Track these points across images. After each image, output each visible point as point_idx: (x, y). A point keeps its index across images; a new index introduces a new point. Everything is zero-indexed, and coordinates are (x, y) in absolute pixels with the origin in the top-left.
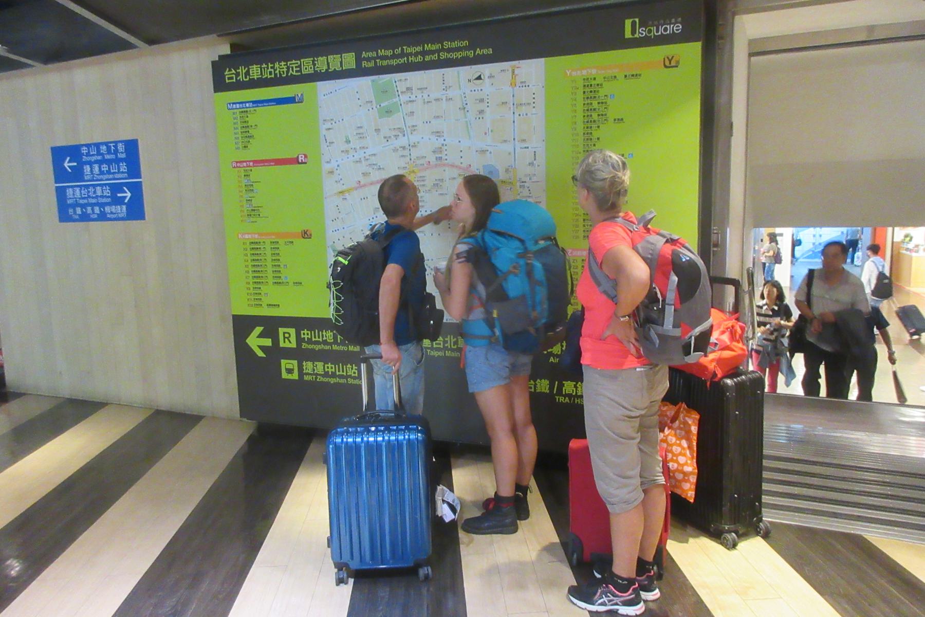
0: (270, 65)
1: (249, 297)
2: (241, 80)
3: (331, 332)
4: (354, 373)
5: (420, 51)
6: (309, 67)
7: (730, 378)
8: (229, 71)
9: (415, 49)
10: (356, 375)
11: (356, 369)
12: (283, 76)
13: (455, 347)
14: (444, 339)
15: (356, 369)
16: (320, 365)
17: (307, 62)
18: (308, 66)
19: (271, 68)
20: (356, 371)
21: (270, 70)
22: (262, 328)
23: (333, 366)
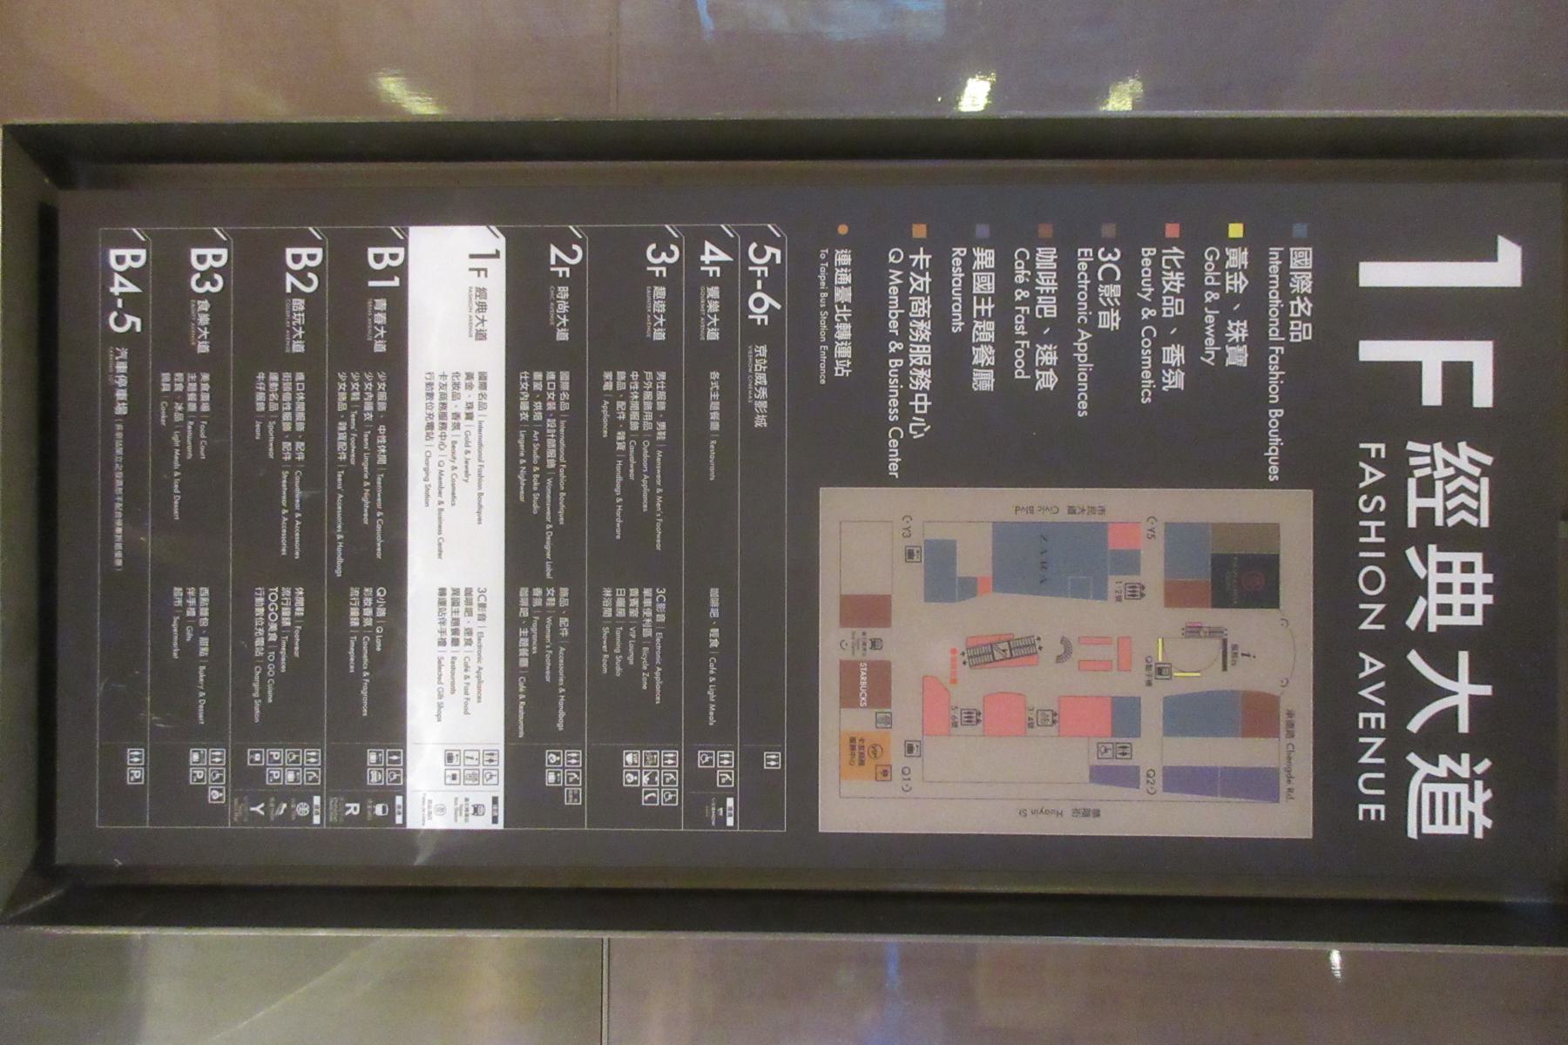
0: (765, 368)
1: (449, 592)
6: (1299, 334)
7: (254, 641)
11: (845, 373)
13: (836, 319)
15: (845, 373)
16: (1052, 286)
20: (842, 375)
23: (925, 411)
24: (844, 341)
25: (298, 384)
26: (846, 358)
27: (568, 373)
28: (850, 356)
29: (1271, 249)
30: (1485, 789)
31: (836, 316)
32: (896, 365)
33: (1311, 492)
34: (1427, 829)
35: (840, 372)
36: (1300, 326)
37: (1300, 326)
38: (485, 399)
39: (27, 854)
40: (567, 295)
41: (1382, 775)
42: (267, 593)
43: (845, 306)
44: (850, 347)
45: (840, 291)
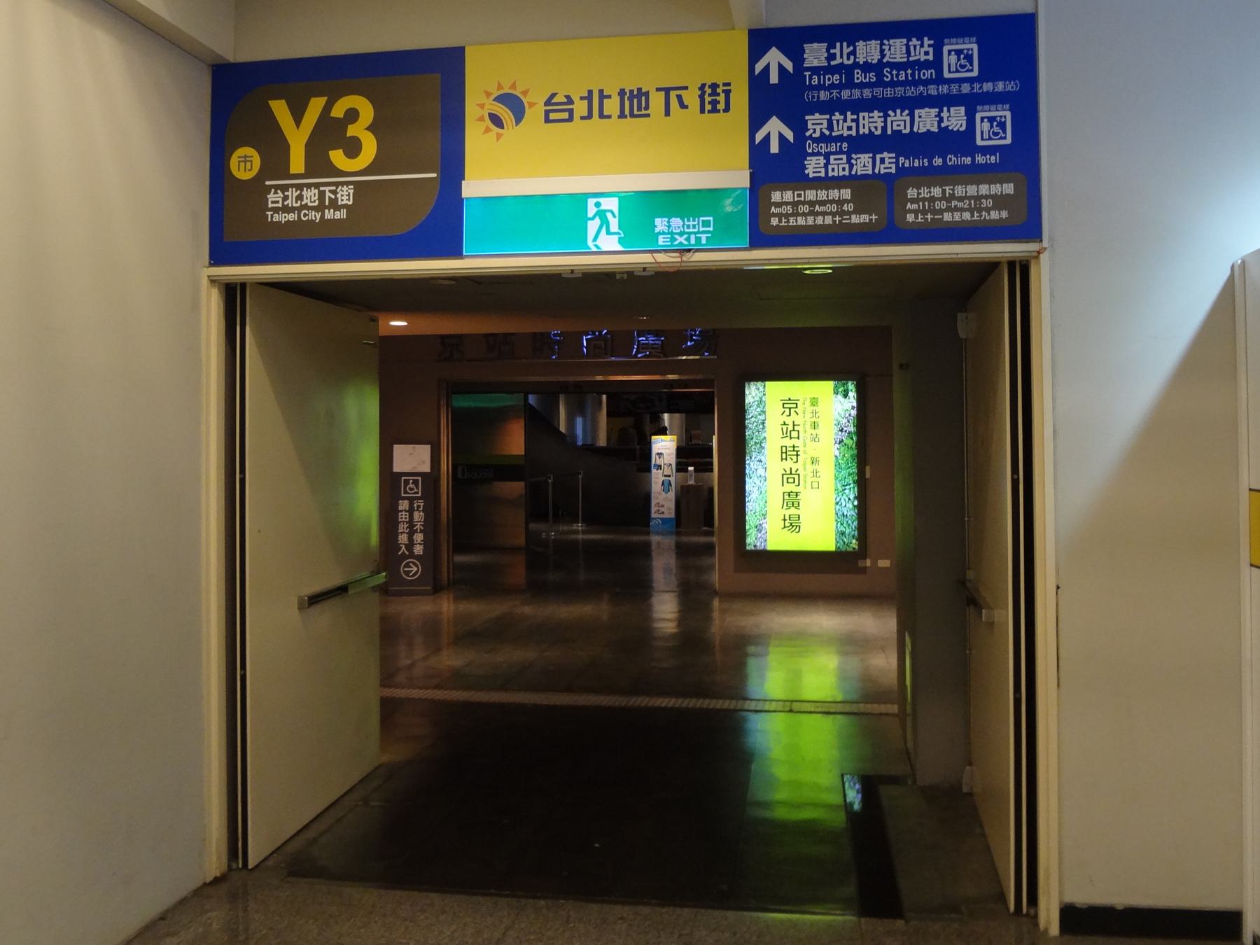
3: (315, 189)
5: (292, 219)
6: (841, 167)
8: (275, 193)
9: (285, 217)
12: (876, 133)
14: (284, 194)
15: (929, 46)
17: (959, 115)
18: (838, 165)
19: (853, 120)
21: (849, 123)
22: (791, 140)
25: (796, 199)
26: (908, 46)
28: (905, 41)
29: (345, 210)
30: (835, 115)
32: (859, 76)
33: (349, 126)
35: (927, 53)
36: (833, 166)
37: (833, 166)
41: (917, 78)
43: (832, 51)
44: (891, 41)
45: (811, 59)
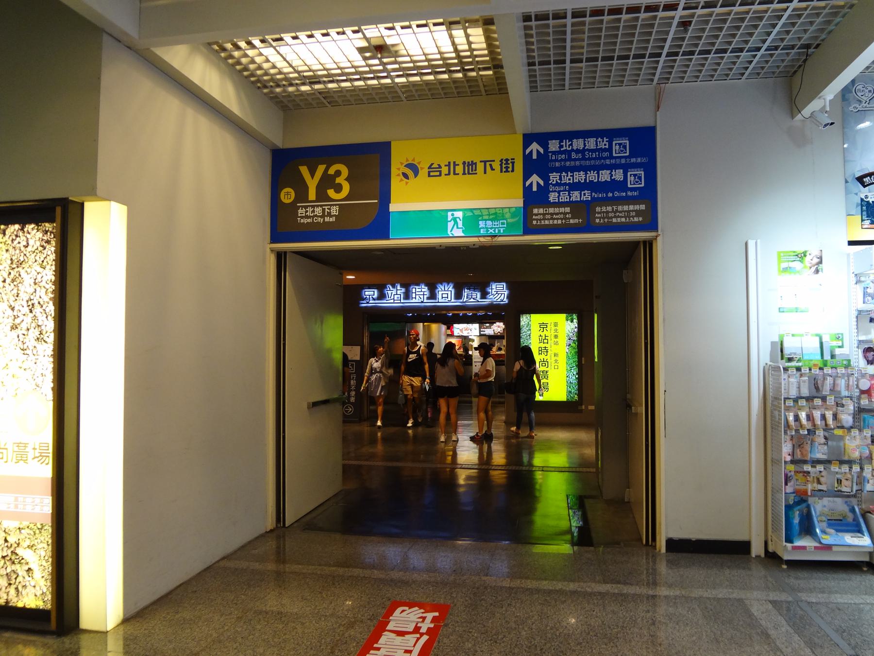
0: (569, 174)
2: (567, 141)
4: (605, 145)
10: (607, 147)
11: (606, 141)
15: (606, 141)
19: (571, 176)
20: (607, 143)
21: (569, 177)
22: (543, 185)
24: (585, 144)
26: (596, 141)
27: (535, 175)
28: (595, 139)
31: (568, 149)
34: (551, 177)
38: (547, 379)
39: (106, 30)
40: (582, 173)
42: (552, 161)
44: (589, 139)
